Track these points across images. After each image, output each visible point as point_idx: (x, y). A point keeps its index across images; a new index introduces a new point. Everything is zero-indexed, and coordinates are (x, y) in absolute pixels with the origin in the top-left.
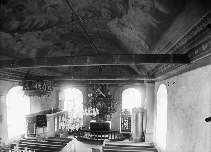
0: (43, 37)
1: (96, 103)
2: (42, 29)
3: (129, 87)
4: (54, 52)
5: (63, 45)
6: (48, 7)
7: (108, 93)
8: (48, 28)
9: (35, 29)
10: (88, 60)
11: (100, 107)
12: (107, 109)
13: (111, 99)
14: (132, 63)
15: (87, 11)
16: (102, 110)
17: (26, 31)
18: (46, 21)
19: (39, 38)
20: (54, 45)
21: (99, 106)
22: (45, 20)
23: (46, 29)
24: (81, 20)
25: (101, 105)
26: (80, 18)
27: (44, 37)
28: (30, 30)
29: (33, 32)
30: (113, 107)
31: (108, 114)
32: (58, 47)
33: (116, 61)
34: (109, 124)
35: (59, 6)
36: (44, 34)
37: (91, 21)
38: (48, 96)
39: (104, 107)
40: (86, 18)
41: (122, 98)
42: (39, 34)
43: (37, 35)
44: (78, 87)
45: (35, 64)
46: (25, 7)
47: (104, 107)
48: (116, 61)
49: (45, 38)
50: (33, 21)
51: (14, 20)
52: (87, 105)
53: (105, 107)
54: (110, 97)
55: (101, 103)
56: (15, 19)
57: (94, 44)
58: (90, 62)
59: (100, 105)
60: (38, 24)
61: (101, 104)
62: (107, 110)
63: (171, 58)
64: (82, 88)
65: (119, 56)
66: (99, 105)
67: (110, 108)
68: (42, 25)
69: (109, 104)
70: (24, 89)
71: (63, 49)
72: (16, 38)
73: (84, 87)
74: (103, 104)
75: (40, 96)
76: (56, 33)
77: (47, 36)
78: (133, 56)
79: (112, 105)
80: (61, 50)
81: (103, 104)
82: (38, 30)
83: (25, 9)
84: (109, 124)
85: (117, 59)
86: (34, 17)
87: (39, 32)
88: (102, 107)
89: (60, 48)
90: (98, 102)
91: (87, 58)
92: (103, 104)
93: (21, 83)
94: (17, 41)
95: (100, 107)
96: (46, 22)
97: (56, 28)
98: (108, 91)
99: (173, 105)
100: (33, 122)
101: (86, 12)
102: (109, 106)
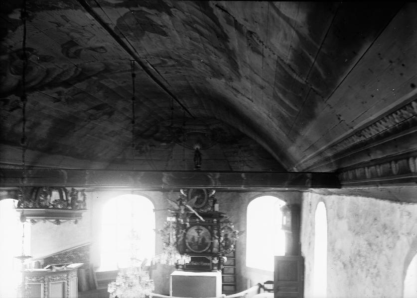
0: (68, 98)
2: (67, 84)
3: (264, 193)
4: (89, 122)
5: (111, 107)
6: (83, 50)
7: (213, 207)
8: (79, 81)
9: (51, 85)
10: (164, 180)
13: (222, 220)
15: (165, 58)
17: (33, 89)
18: (77, 69)
19: (58, 100)
20: (92, 109)
22: (74, 69)
23: (75, 83)
24: (152, 69)
26: (150, 66)
27: (70, 97)
28: (41, 87)
29: (47, 91)
30: (226, 239)
31: (214, 255)
32: (100, 111)
33: (213, 182)
34: (215, 277)
35: (105, 49)
36: (69, 91)
37: (173, 71)
38: (76, 222)
39: (203, 239)
40: (162, 66)
42: (59, 93)
43: (55, 95)
44: (143, 192)
46: (35, 51)
47: (203, 239)
48: (213, 182)
49: (72, 98)
50: (48, 72)
51: (10, 74)
53: (208, 241)
54: (219, 216)
55: (198, 230)
56: (12, 73)
57: (182, 103)
58: (167, 183)
59: (196, 234)
60: (60, 75)
61: (198, 233)
62: (212, 247)
63: (308, 180)
64: (153, 193)
65: (218, 173)
67: (220, 244)
68: (68, 77)
69: (216, 232)
70: (19, 205)
71: (110, 114)
72: (9, 104)
73: (158, 192)
74: (204, 231)
75: (58, 222)
76: (96, 88)
77: (76, 94)
78: (243, 175)
79: (222, 235)
80: (105, 117)
81: (203, 232)
82: (59, 86)
83: (35, 54)
84: (215, 277)
85: (215, 179)
86: (50, 66)
87: (60, 89)
88: (200, 239)
89: (104, 114)
91: (163, 176)
92: (202, 233)
93: (12, 193)
94: (12, 110)
96: (75, 72)
98: (215, 202)
99: (333, 250)
100: (39, 281)
101: (162, 58)
102: (216, 238)
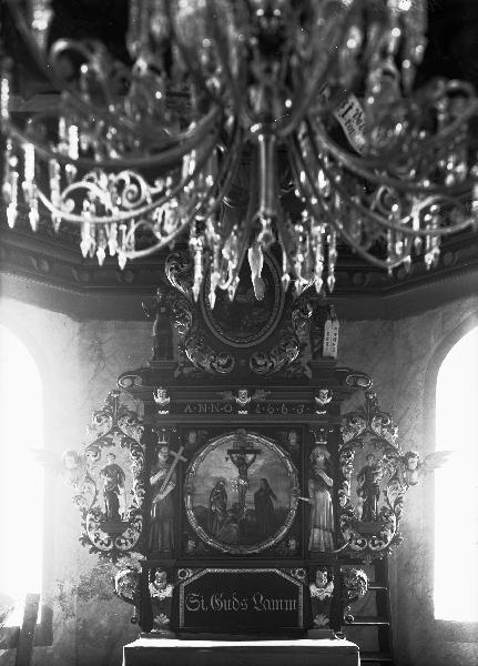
1: (191, 454)
11: (232, 493)
12: (305, 511)
14: (238, 25)
16: (243, 524)
21: (220, 486)
25: (243, 474)
39: (265, 495)
41: (438, 367)
45: (159, 246)
47: (265, 495)
52: (89, 478)
53: (286, 500)
55: (240, 456)
59: (230, 473)
61: (242, 466)
66: (216, 473)
70: (437, 467)
88: (250, 496)
90: (203, 443)
95: (232, 493)
97: (151, 36)
102: (322, 485)
